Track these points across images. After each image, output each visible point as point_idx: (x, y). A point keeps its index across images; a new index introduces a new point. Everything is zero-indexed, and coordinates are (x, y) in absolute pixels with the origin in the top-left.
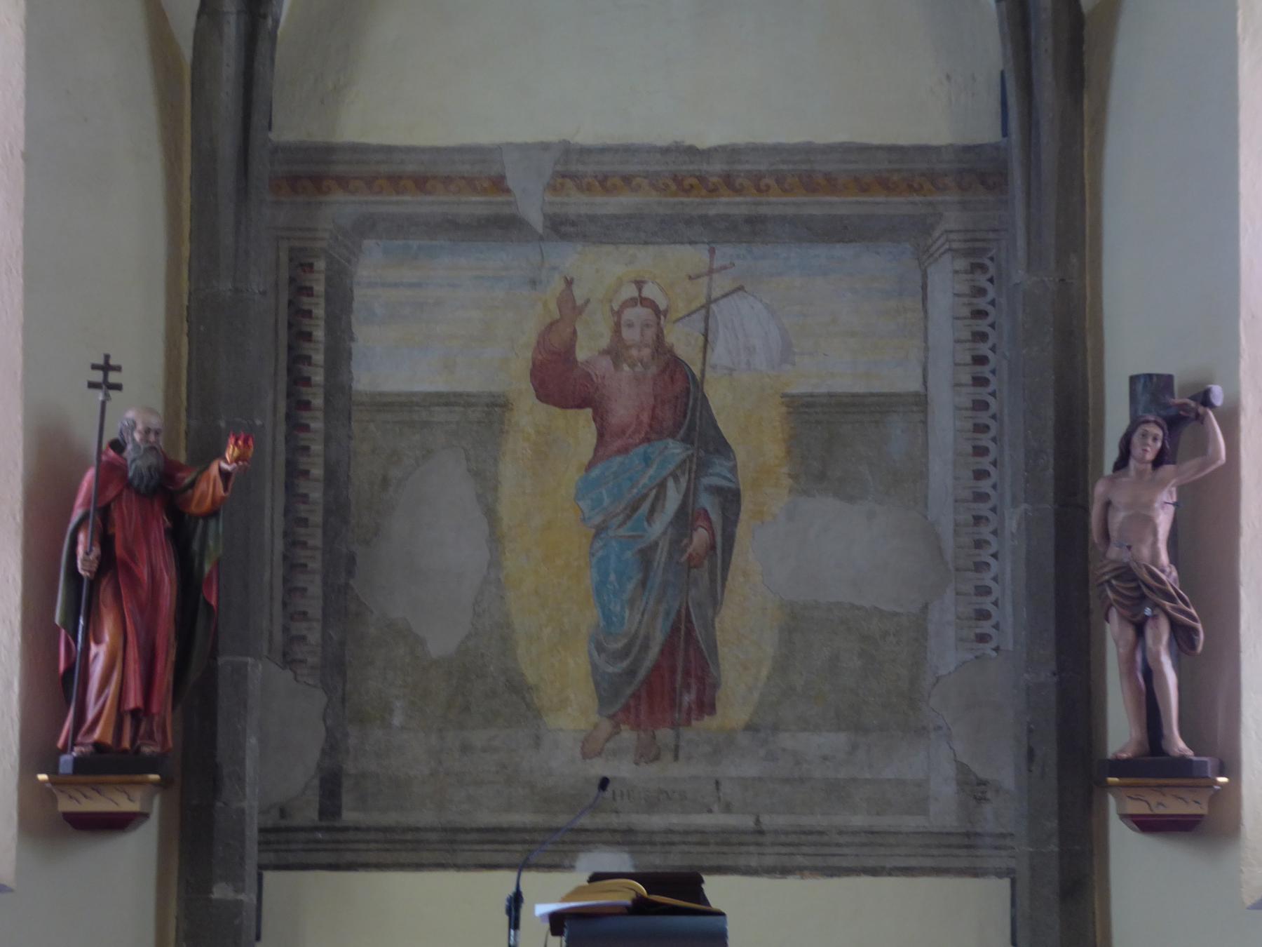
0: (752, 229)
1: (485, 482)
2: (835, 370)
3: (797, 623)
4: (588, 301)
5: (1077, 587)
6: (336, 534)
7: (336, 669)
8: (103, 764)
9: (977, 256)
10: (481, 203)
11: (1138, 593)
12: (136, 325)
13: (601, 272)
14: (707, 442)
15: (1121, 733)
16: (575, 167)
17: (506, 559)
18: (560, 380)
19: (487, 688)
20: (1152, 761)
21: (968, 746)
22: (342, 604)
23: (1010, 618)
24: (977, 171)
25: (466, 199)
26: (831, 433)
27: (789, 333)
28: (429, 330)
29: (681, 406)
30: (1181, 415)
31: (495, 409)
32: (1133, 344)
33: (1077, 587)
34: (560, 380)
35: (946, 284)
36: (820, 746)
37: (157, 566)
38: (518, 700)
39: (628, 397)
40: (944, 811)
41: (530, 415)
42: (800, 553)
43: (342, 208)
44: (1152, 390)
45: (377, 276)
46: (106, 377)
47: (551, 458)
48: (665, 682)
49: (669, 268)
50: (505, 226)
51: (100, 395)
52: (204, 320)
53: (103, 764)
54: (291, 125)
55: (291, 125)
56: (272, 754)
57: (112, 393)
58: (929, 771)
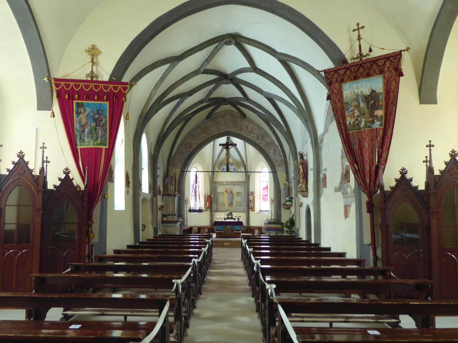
0: (234, 185)
1: (223, 196)
2: (238, 191)
3: (237, 202)
4: (45, 161)
5: (248, 201)
6: (217, 198)
7: (217, 204)
8: (208, 208)
9: (244, 186)
10: (372, 322)
11: (251, 201)
12: (208, 190)
13: (228, 187)
14: (233, 194)
15: (250, 207)
16: (227, 182)
17: (224, 199)
18: (226, 191)
19: (223, 205)
20: (251, 208)
21: (244, 207)
22: (217, 201)
23: (246, 202)
24: (244, 182)
25: (222, 183)
26: (238, 194)
27: (236, 189)
28: (220, 189)
29: (232, 193)
30: (253, 193)
31: (223, 193)
32: (251, 190)
33: (248, 201)
34: (226, 191)
35: (243, 187)
36: (237, 207)
37: (210, 200)
38: (225, 205)
39: (229, 192)
40: (243, 210)
41: (225, 193)
42: (237, 199)
43: (217, 184)
44: (252, 192)
45: (218, 187)
46: (426, 157)
47: (226, 195)
48: (231, 204)
49: (231, 186)
50: (224, 185)
51: (429, 148)
52: (211, 189)
53: (208, 208)
54: (215, 180)
55: (215, 180)
56: (214, 207)
57: (432, 148)
58: (242, 208)
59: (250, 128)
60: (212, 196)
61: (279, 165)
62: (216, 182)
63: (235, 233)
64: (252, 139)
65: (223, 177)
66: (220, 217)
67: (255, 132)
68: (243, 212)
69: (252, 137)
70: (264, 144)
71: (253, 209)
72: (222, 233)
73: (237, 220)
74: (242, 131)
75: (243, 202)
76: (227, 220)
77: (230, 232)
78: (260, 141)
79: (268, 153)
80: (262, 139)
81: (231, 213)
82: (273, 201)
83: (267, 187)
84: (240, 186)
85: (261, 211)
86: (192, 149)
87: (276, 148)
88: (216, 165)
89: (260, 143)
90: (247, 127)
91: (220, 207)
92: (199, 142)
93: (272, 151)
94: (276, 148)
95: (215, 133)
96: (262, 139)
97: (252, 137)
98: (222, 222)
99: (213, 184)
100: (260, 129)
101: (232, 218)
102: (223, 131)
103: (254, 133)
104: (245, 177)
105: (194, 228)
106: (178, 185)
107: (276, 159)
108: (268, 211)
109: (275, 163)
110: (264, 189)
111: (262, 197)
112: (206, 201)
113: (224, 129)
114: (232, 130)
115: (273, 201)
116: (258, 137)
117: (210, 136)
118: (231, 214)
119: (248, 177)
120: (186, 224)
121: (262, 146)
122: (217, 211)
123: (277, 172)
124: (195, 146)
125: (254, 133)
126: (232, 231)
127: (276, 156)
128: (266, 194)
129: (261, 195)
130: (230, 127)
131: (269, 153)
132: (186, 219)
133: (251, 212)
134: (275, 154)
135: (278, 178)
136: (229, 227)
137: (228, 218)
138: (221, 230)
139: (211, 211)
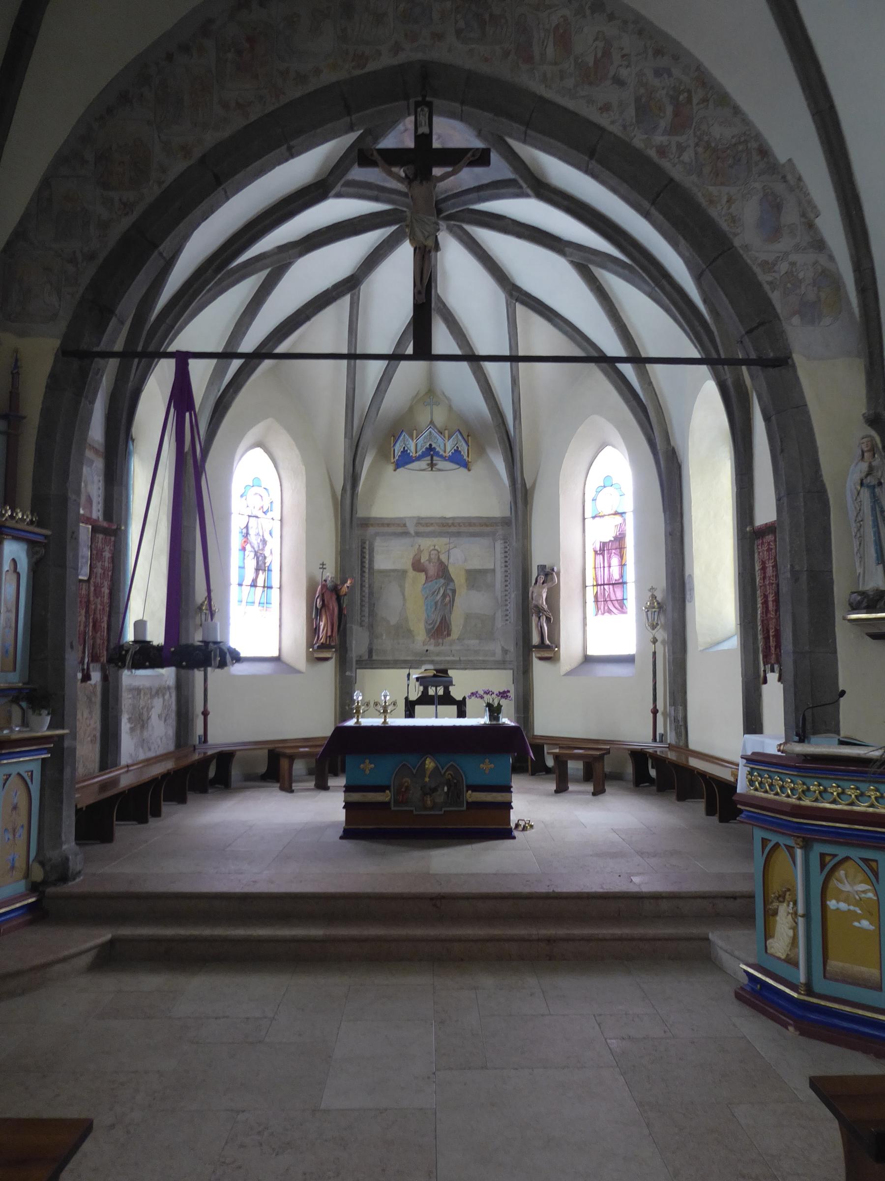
0: (458, 534)
3: (468, 617)
6: (370, 599)
7: (371, 627)
9: (505, 540)
11: (539, 611)
12: (329, 555)
13: (426, 543)
14: (449, 579)
15: (536, 640)
16: (421, 522)
17: (406, 604)
18: (418, 566)
19: (403, 631)
20: (542, 646)
21: (503, 642)
22: (372, 613)
24: (505, 522)
25: (398, 528)
26: (475, 577)
27: (465, 556)
28: (389, 556)
29: (443, 572)
30: (548, 574)
31: (404, 572)
32: (538, 558)
34: (418, 566)
35: (499, 545)
36: (473, 643)
37: (334, 605)
38: (409, 634)
39: (432, 569)
40: (499, 656)
41: (411, 573)
42: (469, 603)
43: (371, 530)
44: (542, 568)
47: (416, 583)
48: (440, 629)
49: (440, 543)
50: (406, 534)
52: (343, 554)
54: (361, 513)
55: (361, 513)
56: (358, 644)
58: (496, 648)
59: (586, 41)
60: (344, 589)
61: (809, 312)
62: (366, 523)
63: (472, 805)
64: (603, 120)
65: (408, 495)
66: (386, 699)
67: (624, 73)
68: (500, 665)
69: (606, 108)
70: (687, 156)
71: (549, 650)
72: (385, 805)
73: (477, 719)
74: (529, 59)
75: (499, 614)
76: (425, 719)
77: (440, 798)
78: (659, 139)
79: (724, 226)
80: (679, 125)
81: (445, 672)
82: (660, 606)
83: (619, 540)
84: (485, 542)
85: (588, 660)
86: (152, 192)
87: (780, 188)
88: (368, 434)
89: (662, 151)
90: (564, 39)
91: (386, 644)
92: (211, 138)
93: (750, 211)
94: (780, 188)
95: (328, 77)
96: (679, 125)
97: (606, 108)
98: (385, 731)
99: (351, 527)
100: (659, 52)
101: (447, 699)
102: (387, 60)
103: (619, 82)
104: (508, 497)
105: (238, 753)
106: (42, 457)
107: (784, 267)
108: (629, 660)
109: (775, 297)
110: (603, 549)
111: (590, 593)
112: (315, 612)
113: (397, 48)
114: (455, 52)
115: (660, 606)
116: (645, 110)
117: (297, 93)
118: (441, 676)
119: (522, 495)
120: (200, 731)
121: (677, 173)
122: (371, 661)
123: (797, 358)
124: (179, 166)
125: (619, 82)
126: (456, 790)
127: (784, 244)
128: (616, 576)
129: (590, 581)
130: (439, 37)
131: (734, 220)
132: (199, 708)
133: (539, 668)
134: (775, 233)
135: (802, 407)
136: (430, 764)
137: (425, 699)
138: (381, 789)
139: (343, 665)
